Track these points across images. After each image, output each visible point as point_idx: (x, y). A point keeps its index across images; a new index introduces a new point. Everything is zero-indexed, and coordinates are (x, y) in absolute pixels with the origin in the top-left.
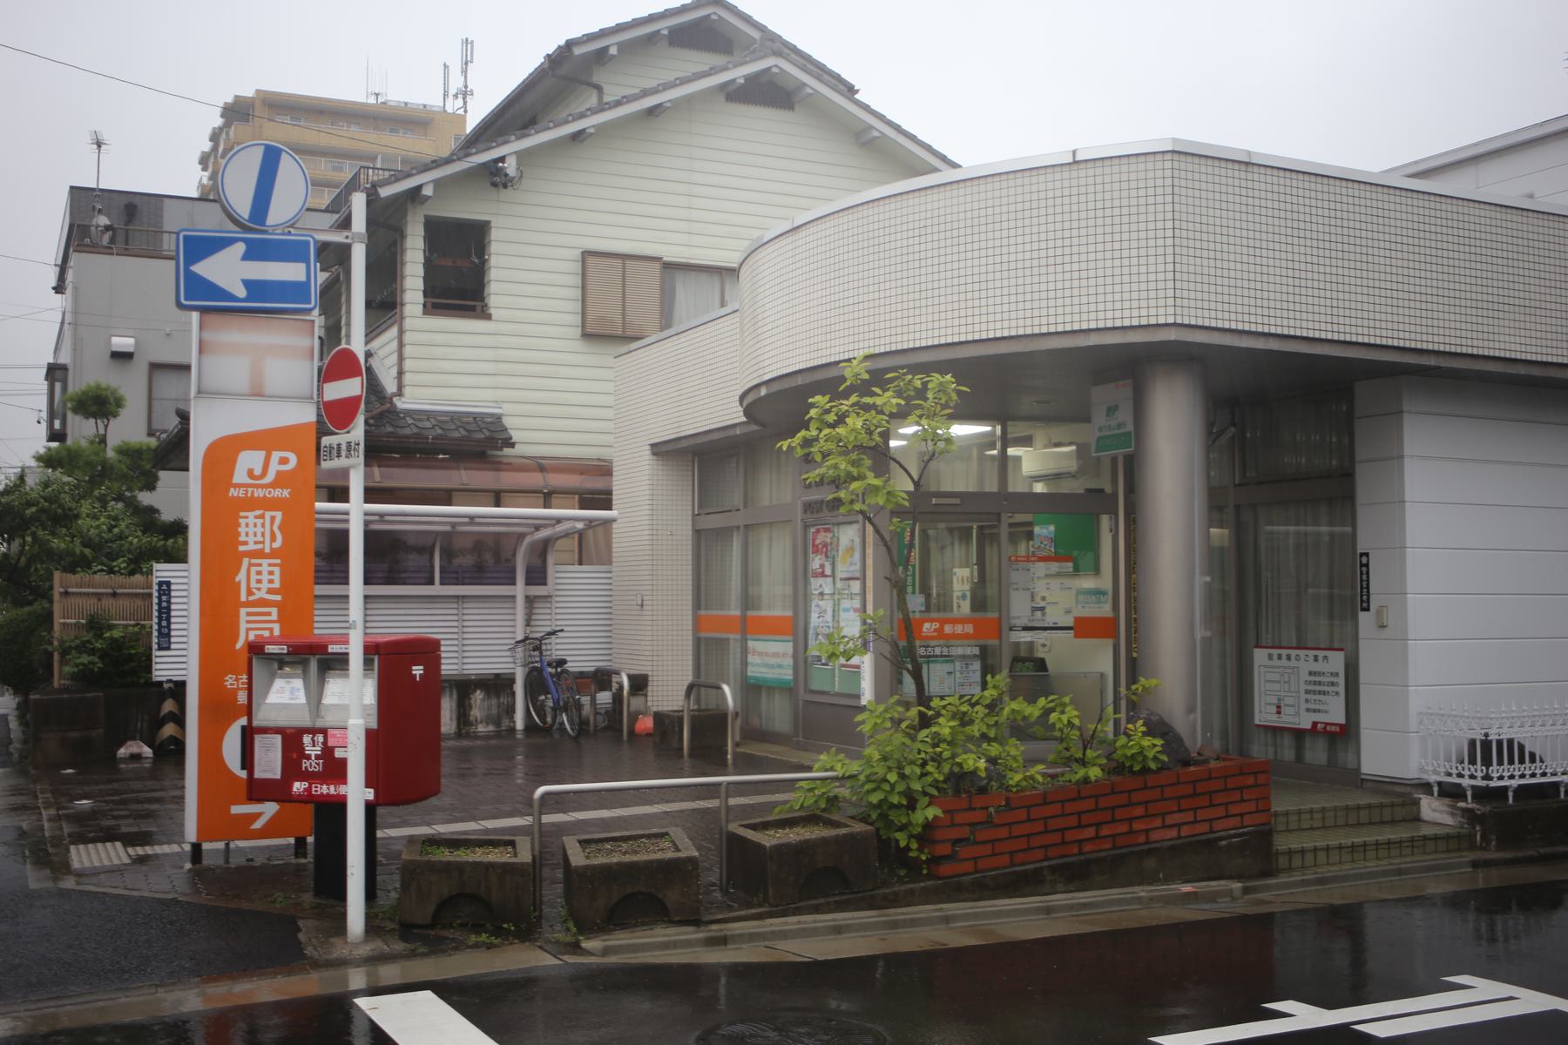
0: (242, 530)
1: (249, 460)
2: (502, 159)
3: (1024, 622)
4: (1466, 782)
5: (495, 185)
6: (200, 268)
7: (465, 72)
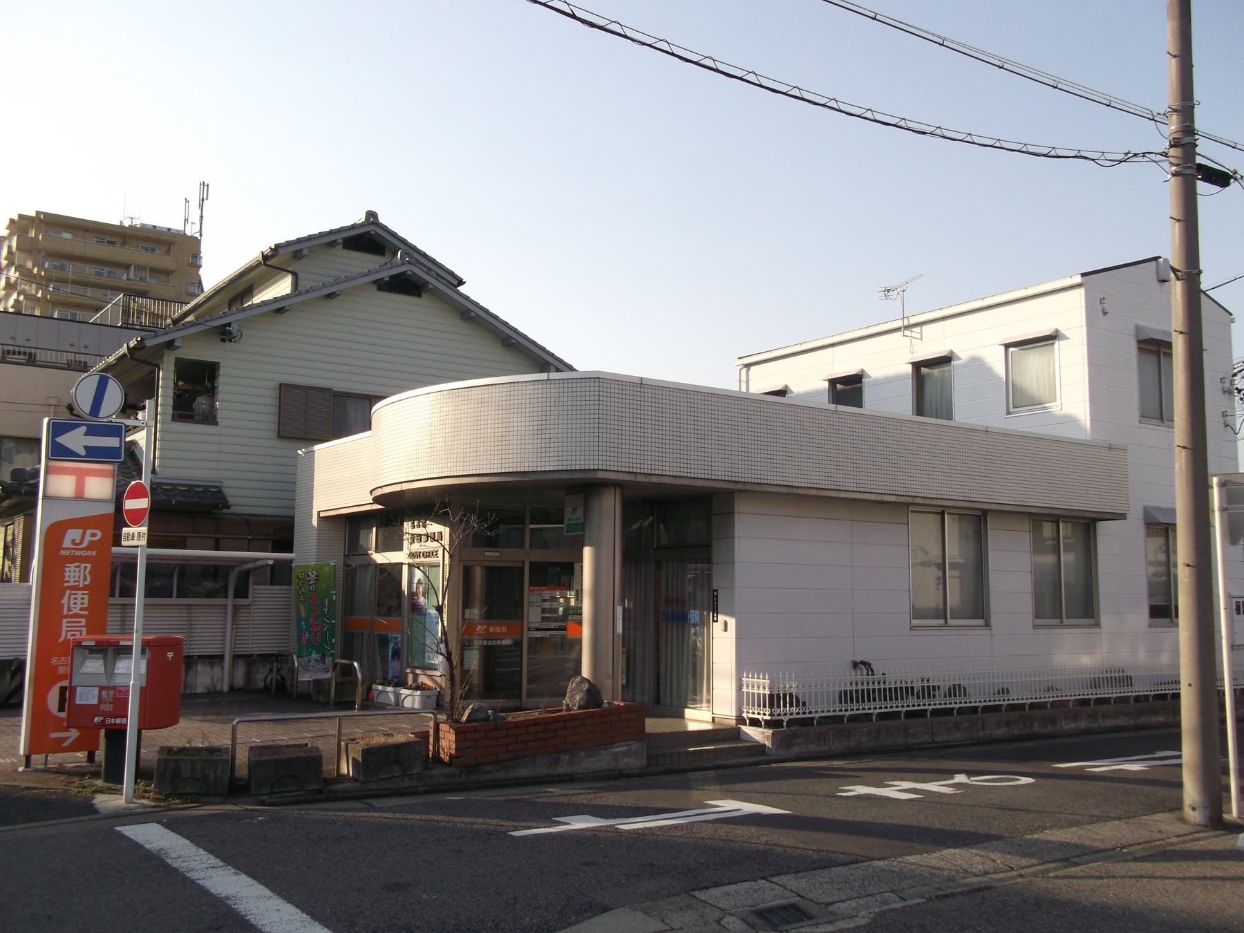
0: (67, 574)
1: (73, 534)
2: (229, 324)
3: (537, 625)
4: (760, 717)
5: (223, 340)
6: (57, 440)
7: (201, 206)
